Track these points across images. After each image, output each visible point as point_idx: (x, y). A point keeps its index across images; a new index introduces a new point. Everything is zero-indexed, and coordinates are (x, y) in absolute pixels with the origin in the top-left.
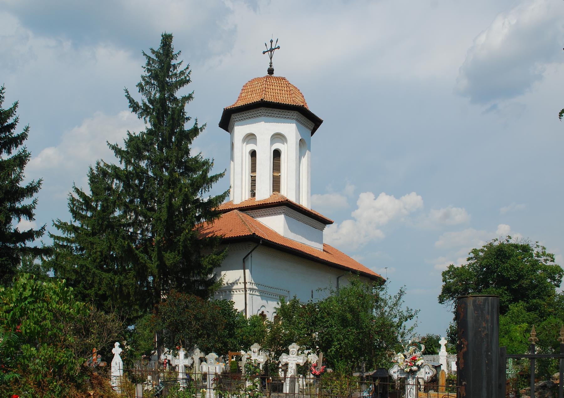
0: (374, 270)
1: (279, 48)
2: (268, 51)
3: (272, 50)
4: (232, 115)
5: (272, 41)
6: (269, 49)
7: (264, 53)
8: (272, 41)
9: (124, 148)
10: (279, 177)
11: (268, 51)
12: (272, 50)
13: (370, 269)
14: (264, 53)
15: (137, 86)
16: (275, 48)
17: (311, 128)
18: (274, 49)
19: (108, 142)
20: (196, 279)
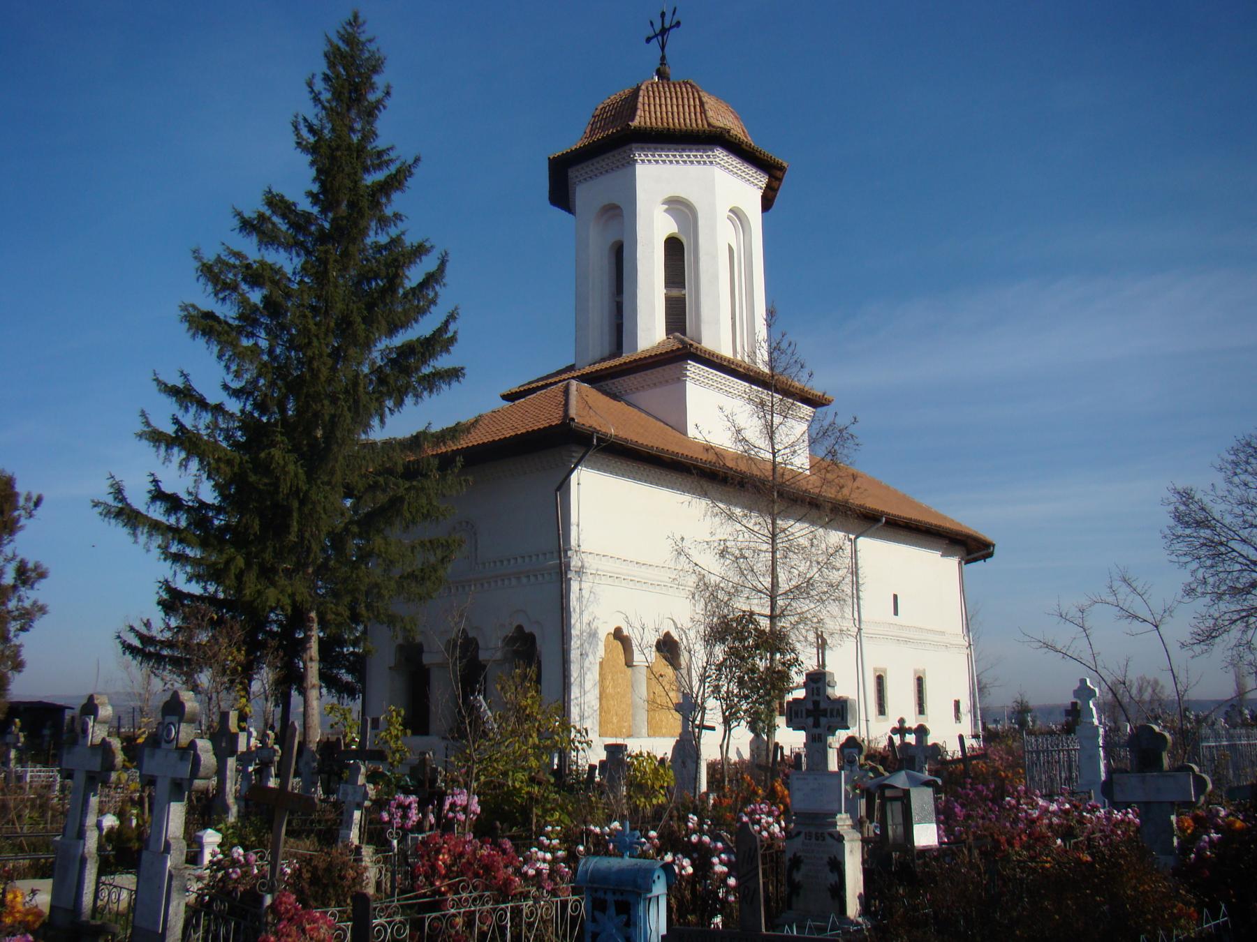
0: (969, 565)
1: (678, 24)
2: (656, 36)
3: (664, 31)
4: (570, 170)
5: (663, 15)
6: (658, 30)
7: (648, 40)
8: (663, 15)
9: (207, 337)
10: (681, 301)
11: (656, 36)
12: (664, 31)
13: (918, 499)
14: (648, 40)
15: (296, 149)
16: (671, 27)
17: (760, 184)
18: (669, 29)
19: (223, 244)
20: (455, 448)
